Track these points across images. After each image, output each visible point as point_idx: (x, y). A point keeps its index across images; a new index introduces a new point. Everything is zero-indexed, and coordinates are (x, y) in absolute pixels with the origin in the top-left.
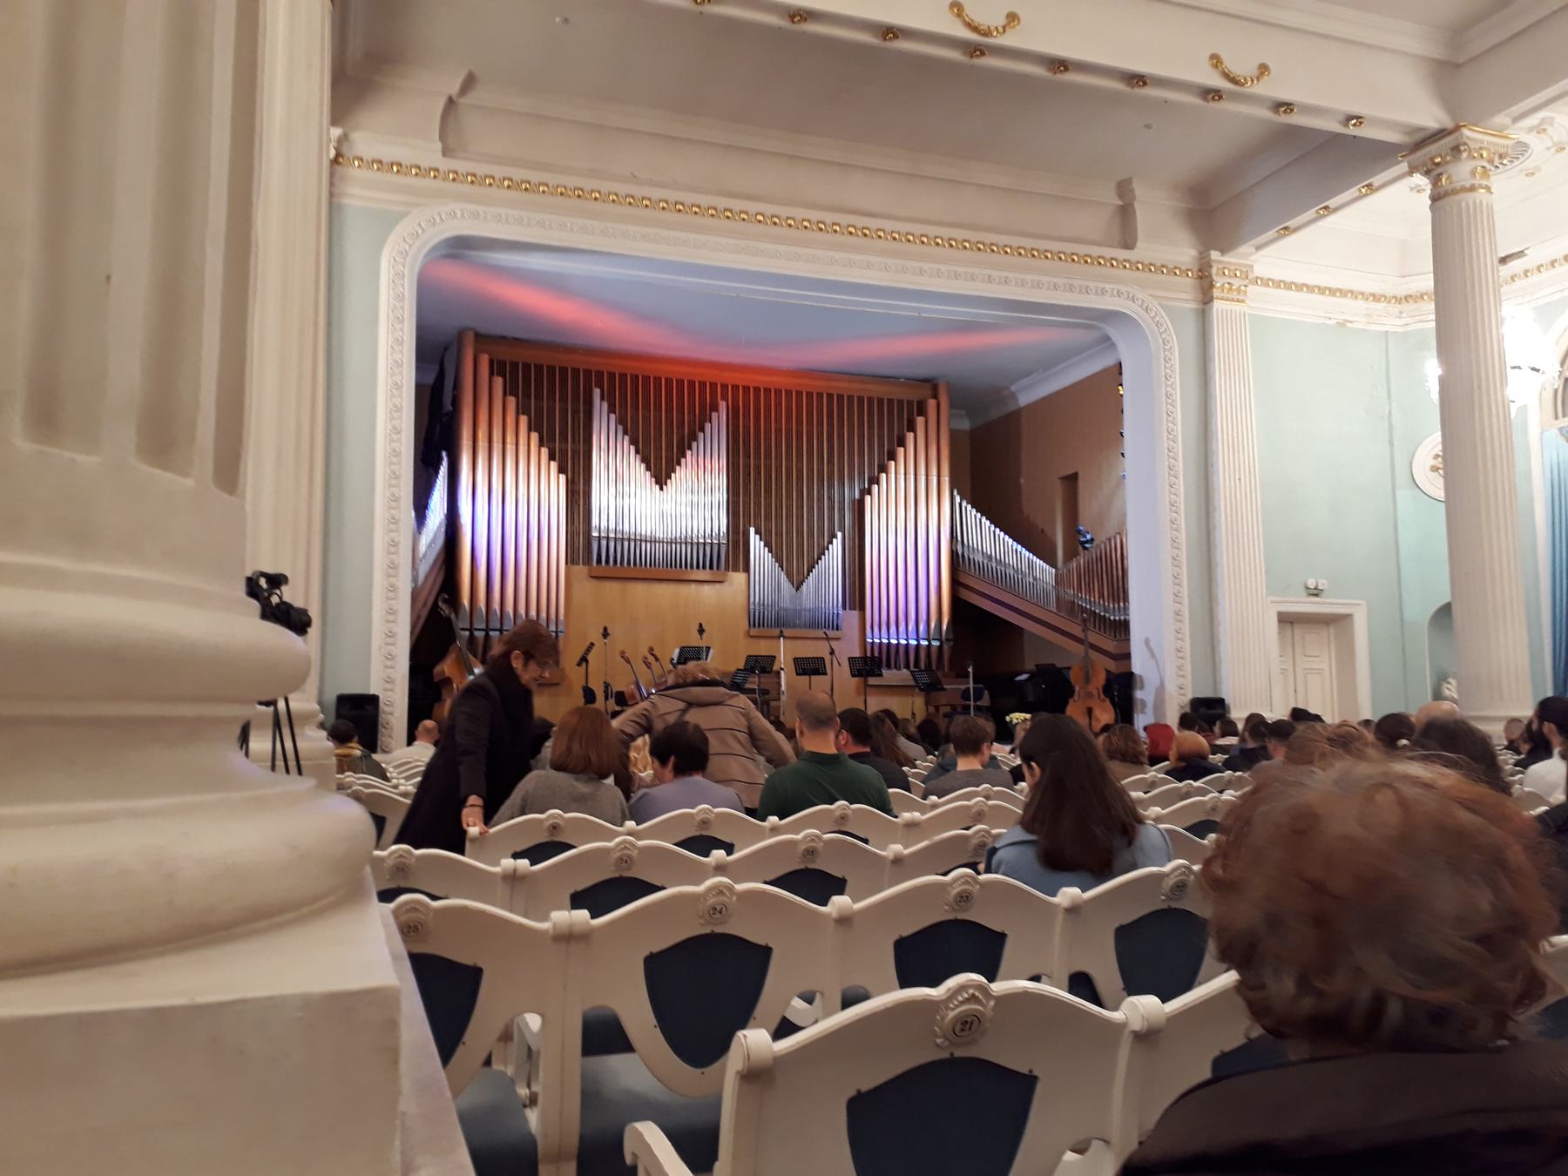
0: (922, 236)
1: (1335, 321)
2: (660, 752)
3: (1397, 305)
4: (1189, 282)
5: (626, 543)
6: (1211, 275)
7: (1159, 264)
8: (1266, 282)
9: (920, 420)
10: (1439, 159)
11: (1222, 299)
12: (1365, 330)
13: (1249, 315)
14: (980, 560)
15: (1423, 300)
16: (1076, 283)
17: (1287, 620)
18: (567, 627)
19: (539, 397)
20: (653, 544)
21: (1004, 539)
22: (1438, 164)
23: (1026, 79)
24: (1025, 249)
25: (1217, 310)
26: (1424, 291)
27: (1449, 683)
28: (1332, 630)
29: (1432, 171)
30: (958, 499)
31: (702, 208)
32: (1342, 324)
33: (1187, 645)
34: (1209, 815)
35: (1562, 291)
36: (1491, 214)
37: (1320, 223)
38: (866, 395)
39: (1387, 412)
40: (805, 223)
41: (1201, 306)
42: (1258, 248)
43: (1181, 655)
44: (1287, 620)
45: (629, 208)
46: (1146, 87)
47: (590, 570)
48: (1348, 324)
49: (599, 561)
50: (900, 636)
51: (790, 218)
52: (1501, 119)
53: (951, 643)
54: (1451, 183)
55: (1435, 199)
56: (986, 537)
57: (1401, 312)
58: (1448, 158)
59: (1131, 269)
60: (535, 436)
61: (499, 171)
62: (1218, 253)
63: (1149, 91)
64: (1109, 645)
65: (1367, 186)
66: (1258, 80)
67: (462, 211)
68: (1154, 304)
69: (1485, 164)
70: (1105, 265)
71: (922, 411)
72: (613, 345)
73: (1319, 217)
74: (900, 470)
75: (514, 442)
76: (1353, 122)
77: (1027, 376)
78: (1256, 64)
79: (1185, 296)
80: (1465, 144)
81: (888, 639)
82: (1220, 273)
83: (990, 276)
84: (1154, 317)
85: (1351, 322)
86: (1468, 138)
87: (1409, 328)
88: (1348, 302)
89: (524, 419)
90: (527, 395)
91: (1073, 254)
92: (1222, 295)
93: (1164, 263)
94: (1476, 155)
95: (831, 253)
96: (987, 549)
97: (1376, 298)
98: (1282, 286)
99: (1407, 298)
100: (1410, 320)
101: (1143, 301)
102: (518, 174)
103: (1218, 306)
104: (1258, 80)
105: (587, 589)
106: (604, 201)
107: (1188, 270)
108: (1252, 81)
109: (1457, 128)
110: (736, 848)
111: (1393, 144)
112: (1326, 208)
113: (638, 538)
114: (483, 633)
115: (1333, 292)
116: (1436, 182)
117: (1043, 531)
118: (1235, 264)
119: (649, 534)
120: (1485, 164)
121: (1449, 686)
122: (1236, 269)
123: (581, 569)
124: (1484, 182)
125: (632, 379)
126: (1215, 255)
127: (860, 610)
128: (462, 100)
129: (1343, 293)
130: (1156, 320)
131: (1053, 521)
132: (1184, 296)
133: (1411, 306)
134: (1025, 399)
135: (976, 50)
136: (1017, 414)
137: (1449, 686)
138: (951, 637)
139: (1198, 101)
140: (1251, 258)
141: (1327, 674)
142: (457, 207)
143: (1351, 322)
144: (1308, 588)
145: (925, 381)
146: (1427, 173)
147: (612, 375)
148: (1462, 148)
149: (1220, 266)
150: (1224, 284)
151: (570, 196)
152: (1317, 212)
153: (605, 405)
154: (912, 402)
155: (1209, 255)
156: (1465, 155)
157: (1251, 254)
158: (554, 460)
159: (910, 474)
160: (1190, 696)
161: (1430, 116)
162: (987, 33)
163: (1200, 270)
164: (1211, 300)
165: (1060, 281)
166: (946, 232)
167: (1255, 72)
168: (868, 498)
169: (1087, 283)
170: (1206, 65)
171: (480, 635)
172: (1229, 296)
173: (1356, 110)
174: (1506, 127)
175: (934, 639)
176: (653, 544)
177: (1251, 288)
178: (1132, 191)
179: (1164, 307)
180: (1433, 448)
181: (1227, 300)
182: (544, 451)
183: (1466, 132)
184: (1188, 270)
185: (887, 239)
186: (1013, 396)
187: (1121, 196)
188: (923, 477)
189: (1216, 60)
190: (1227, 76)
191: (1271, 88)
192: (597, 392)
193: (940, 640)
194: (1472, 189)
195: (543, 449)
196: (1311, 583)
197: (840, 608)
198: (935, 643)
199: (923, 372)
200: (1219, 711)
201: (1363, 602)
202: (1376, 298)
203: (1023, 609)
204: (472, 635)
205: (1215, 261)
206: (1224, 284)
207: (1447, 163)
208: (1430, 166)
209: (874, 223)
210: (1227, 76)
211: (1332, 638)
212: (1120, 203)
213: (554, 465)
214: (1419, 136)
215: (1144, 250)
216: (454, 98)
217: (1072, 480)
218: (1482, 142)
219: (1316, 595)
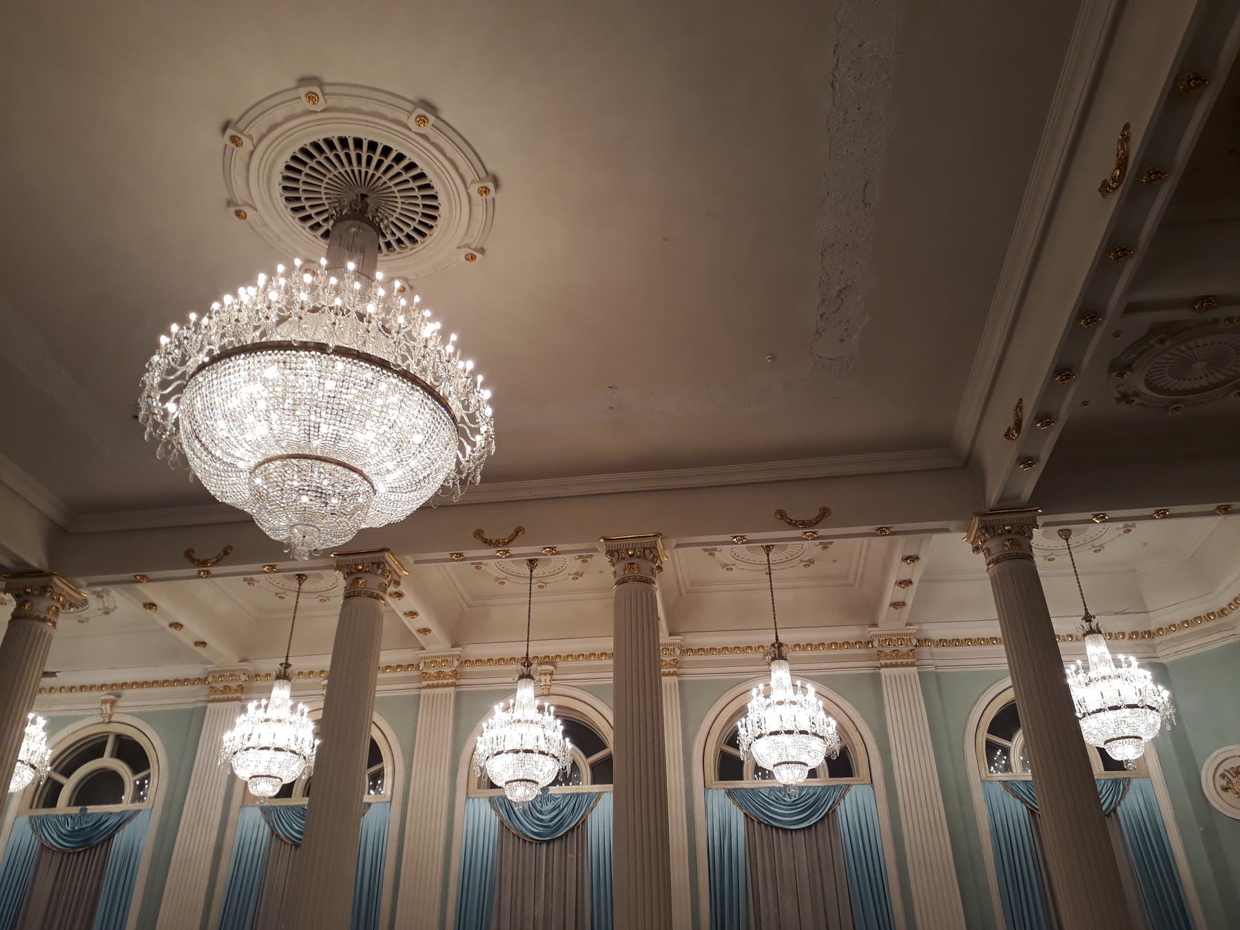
52: (81, 581)
55: (16, 617)
69: (59, 606)
80: (52, 587)
86: (55, 583)
94: (55, 597)
109: (51, 575)
116: (20, 606)
120: (59, 606)
124: (54, 619)
148: (49, 589)
156: (48, 594)
161: (35, 557)
194: (44, 620)
218: (63, 590)
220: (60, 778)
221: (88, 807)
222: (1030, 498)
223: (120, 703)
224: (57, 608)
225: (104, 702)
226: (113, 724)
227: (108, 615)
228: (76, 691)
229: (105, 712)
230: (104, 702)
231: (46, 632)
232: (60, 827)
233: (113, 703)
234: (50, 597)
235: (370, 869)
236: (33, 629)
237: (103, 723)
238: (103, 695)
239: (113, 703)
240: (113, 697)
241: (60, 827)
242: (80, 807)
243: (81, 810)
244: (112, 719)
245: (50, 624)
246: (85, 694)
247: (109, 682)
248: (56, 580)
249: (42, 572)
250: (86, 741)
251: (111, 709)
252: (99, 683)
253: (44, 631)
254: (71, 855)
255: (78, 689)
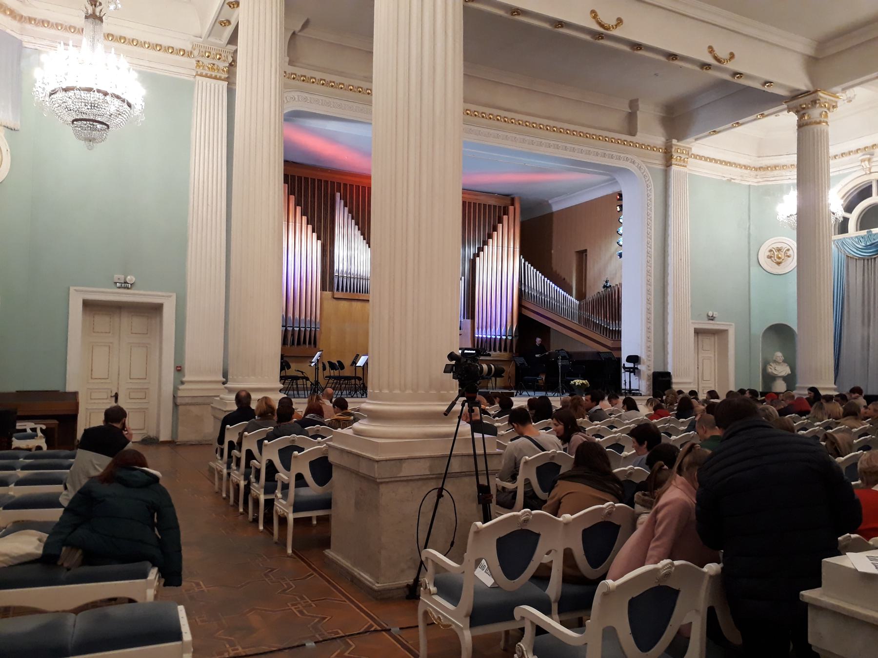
0: (533, 123)
1: (726, 179)
2: (625, 402)
3: (755, 172)
4: (660, 154)
5: (352, 280)
6: (671, 152)
7: (646, 145)
8: (696, 157)
9: (505, 217)
10: (805, 106)
11: (676, 165)
12: (739, 184)
13: (689, 174)
14: (535, 294)
15: (768, 170)
16: (607, 153)
17: (698, 332)
18: (321, 323)
19: (306, 196)
20: (367, 281)
21: (549, 284)
22: (804, 108)
23: (616, 52)
24: (576, 132)
25: (674, 170)
26: (769, 165)
27: (771, 365)
28: (716, 337)
29: (800, 112)
30: (523, 261)
31: (364, 89)
32: (729, 180)
33: (652, 344)
34: (598, 432)
35: (839, 171)
36: (827, 134)
37: (733, 130)
38: (478, 202)
39: (748, 226)
40: (476, 113)
41: (665, 168)
42: (696, 139)
43: (649, 349)
44: (698, 332)
45: (322, 86)
46: (676, 61)
47: (333, 295)
48: (733, 181)
49: (338, 289)
50: (488, 334)
51: (468, 110)
52: (835, 89)
53: (518, 338)
54: (810, 118)
55: (800, 126)
56: (538, 281)
57: (757, 175)
58: (809, 106)
59: (633, 146)
60: (304, 218)
61: (318, 75)
62: (676, 141)
63: (676, 63)
64: (609, 343)
65: (761, 114)
66: (730, 61)
67: (298, 96)
68: (644, 166)
69: (826, 110)
70: (621, 144)
71: (506, 212)
72: (347, 168)
73: (733, 127)
74: (510, 245)
75: (294, 221)
76: (767, 85)
77: (560, 196)
78: (729, 52)
79: (657, 162)
80: (819, 100)
81: (486, 335)
82: (676, 150)
83: (566, 147)
84: (643, 173)
85: (734, 179)
86: (820, 97)
87: (760, 184)
88: (733, 169)
89: (299, 209)
90: (300, 195)
91: (606, 137)
92: (676, 163)
93: (643, 143)
94: (823, 105)
95: (489, 130)
96: (539, 288)
97: (746, 167)
98: (703, 159)
99: (760, 168)
100: (760, 180)
101: (639, 164)
102: (328, 77)
103: (674, 168)
104: (730, 61)
105: (330, 304)
106: (346, 89)
107: (660, 148)
108: (727, 62)
109: (816, 91)
110: (625, 449)
111: (782, 96)
112: (737, 123)
113: (359, 277)
114: (298, 329)
115: (726, 163)
116: (801, 117)
117: (564, 279)
118: (684, 147)
119: (364, 275)
120: (826, 110)
121: (771, 367)
122: (684, 150)
123: (328, 293)
124: (825, 120)
125: (356, 187)
126: (674, 141)
127: (471, 319)
128: (299, 34)
129: (730, 164)
130: (644, 174)
131: (571, 272)
132: (658, 163)
133: (762, 173)
134: (555, 208)
135: (599, 36)
136: (552, 214)
137: (771, 367)
138: (517, 335)
139: (698, 69)
140: (691, 144)
141: (713, 359)
142: (296, 94)
143: (734, 179)
144: (708, 316)
145: (507, 195)
146: (797, 112)
147: (345, 185)
148: (818, 102)
149: (677, 147)
150: (684, 159)
151: (355, 91)
152: (733, 125)
153: (342, 202)
154: (496, 206)
155: (671, 142)
156: (818, 105)
157: (692, 142)
158: (314, 232)
159: (505, 247)
160: (652, 371)
161: (802, 83)
162: (608, 29)
163: (666, 149)
164: (671, 165)
165: (600, 151)
166: (546, 122)
167: (728, 57)
168: (478, 259)
169: (605, 152)
170: (706, 51)
171: (303, 329)
172: (680, 163)
173: (771, 79)
174: (837, 93)
175: (509, 336)
176: (367, 281)
177: (690, 160)
178: (638, 105)
179: (647, 167)
180: (769, 247)
181: (678, 165)
182: (310, 227)
183: (820, 94)
184: (660, 148)
185: (516, 124)
186: (550, 206)
187: (630, 107)
188: (506, 248)
189: (711, 50)
190: (716, 58)
191: (732, 66)
192: (338, 195)
193: (512, 336)
194: (820, 123)
195: (309, 226)
196: (710, 314)
197: (462, 318)
198: (510, 338)
199: (506, 191)
200: (667, 379)
201: (733, 324)
202: (746, 167)
203: (561, 322)
204: (293, 329)
205: (674, 145)
206: (684, 159)
207: (808, 108)
208: (799, 109)
209: (510, 115)
210: (716, 58)
211: (716, 340)
212: (630, 111)
213: (315, 235)
214: (796, 93)
215: (640, 137)
216: (296, 32)
217: (582, 255)
218: (826, 99)
219: (712, 320)
220: (847, 215)
221: (872, 230)
222: (472, 641)
223: (874, 159)
224: (826, 112)
225: (863, 161)
226: (873, 174)
227: (851, 102)
228: (839, 158)
229: (865, 167)
230: (863, 161)
231: (824, 130)
232: (856, 244)
233: (869, 160)
234: (819, 107)
235: (861, 288)
236: (815, 131)
237: (866, 174)
238: (859, 156)
239: (869, 160)
240: (869, 156)
241: (856, 244)
242: (866, 231)
243: (867, 232)
244: (872, 171)
245: (824, 124)
246: (846, 159)
247: (862, 147)
248: (820, 94)
249: (810, 91)
250: (856, 188)
251: (869, 165)
252: (854, 148)
253: (822, 129)
254: (870, 261)
255: (833, 158)
